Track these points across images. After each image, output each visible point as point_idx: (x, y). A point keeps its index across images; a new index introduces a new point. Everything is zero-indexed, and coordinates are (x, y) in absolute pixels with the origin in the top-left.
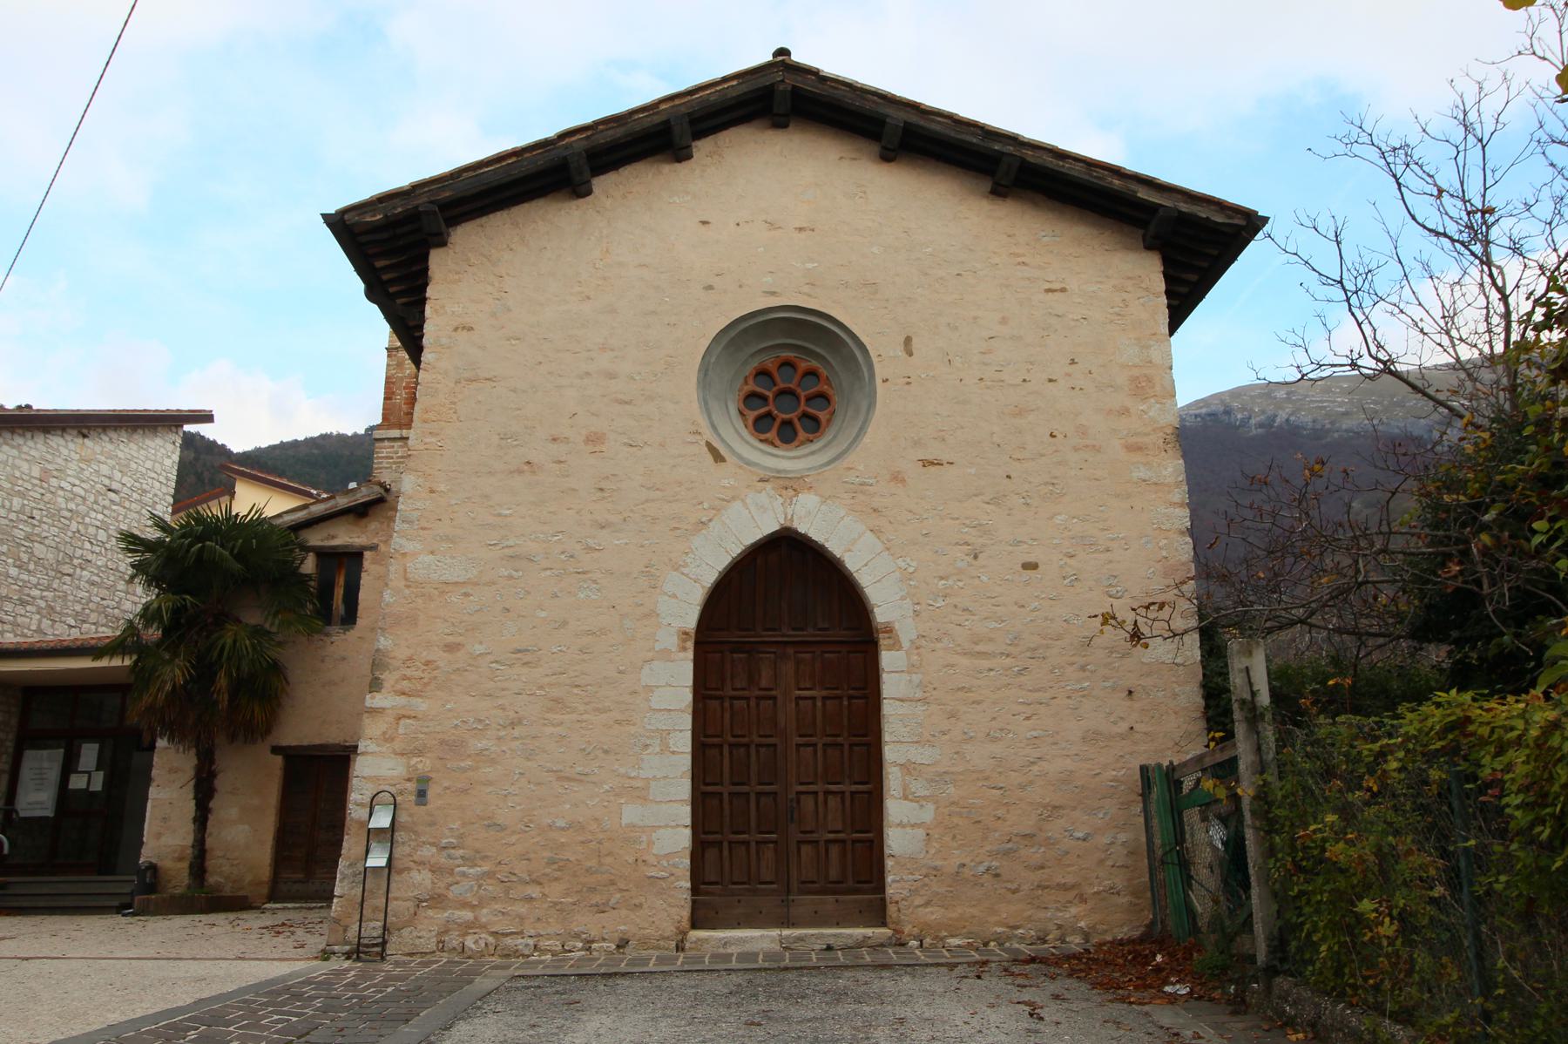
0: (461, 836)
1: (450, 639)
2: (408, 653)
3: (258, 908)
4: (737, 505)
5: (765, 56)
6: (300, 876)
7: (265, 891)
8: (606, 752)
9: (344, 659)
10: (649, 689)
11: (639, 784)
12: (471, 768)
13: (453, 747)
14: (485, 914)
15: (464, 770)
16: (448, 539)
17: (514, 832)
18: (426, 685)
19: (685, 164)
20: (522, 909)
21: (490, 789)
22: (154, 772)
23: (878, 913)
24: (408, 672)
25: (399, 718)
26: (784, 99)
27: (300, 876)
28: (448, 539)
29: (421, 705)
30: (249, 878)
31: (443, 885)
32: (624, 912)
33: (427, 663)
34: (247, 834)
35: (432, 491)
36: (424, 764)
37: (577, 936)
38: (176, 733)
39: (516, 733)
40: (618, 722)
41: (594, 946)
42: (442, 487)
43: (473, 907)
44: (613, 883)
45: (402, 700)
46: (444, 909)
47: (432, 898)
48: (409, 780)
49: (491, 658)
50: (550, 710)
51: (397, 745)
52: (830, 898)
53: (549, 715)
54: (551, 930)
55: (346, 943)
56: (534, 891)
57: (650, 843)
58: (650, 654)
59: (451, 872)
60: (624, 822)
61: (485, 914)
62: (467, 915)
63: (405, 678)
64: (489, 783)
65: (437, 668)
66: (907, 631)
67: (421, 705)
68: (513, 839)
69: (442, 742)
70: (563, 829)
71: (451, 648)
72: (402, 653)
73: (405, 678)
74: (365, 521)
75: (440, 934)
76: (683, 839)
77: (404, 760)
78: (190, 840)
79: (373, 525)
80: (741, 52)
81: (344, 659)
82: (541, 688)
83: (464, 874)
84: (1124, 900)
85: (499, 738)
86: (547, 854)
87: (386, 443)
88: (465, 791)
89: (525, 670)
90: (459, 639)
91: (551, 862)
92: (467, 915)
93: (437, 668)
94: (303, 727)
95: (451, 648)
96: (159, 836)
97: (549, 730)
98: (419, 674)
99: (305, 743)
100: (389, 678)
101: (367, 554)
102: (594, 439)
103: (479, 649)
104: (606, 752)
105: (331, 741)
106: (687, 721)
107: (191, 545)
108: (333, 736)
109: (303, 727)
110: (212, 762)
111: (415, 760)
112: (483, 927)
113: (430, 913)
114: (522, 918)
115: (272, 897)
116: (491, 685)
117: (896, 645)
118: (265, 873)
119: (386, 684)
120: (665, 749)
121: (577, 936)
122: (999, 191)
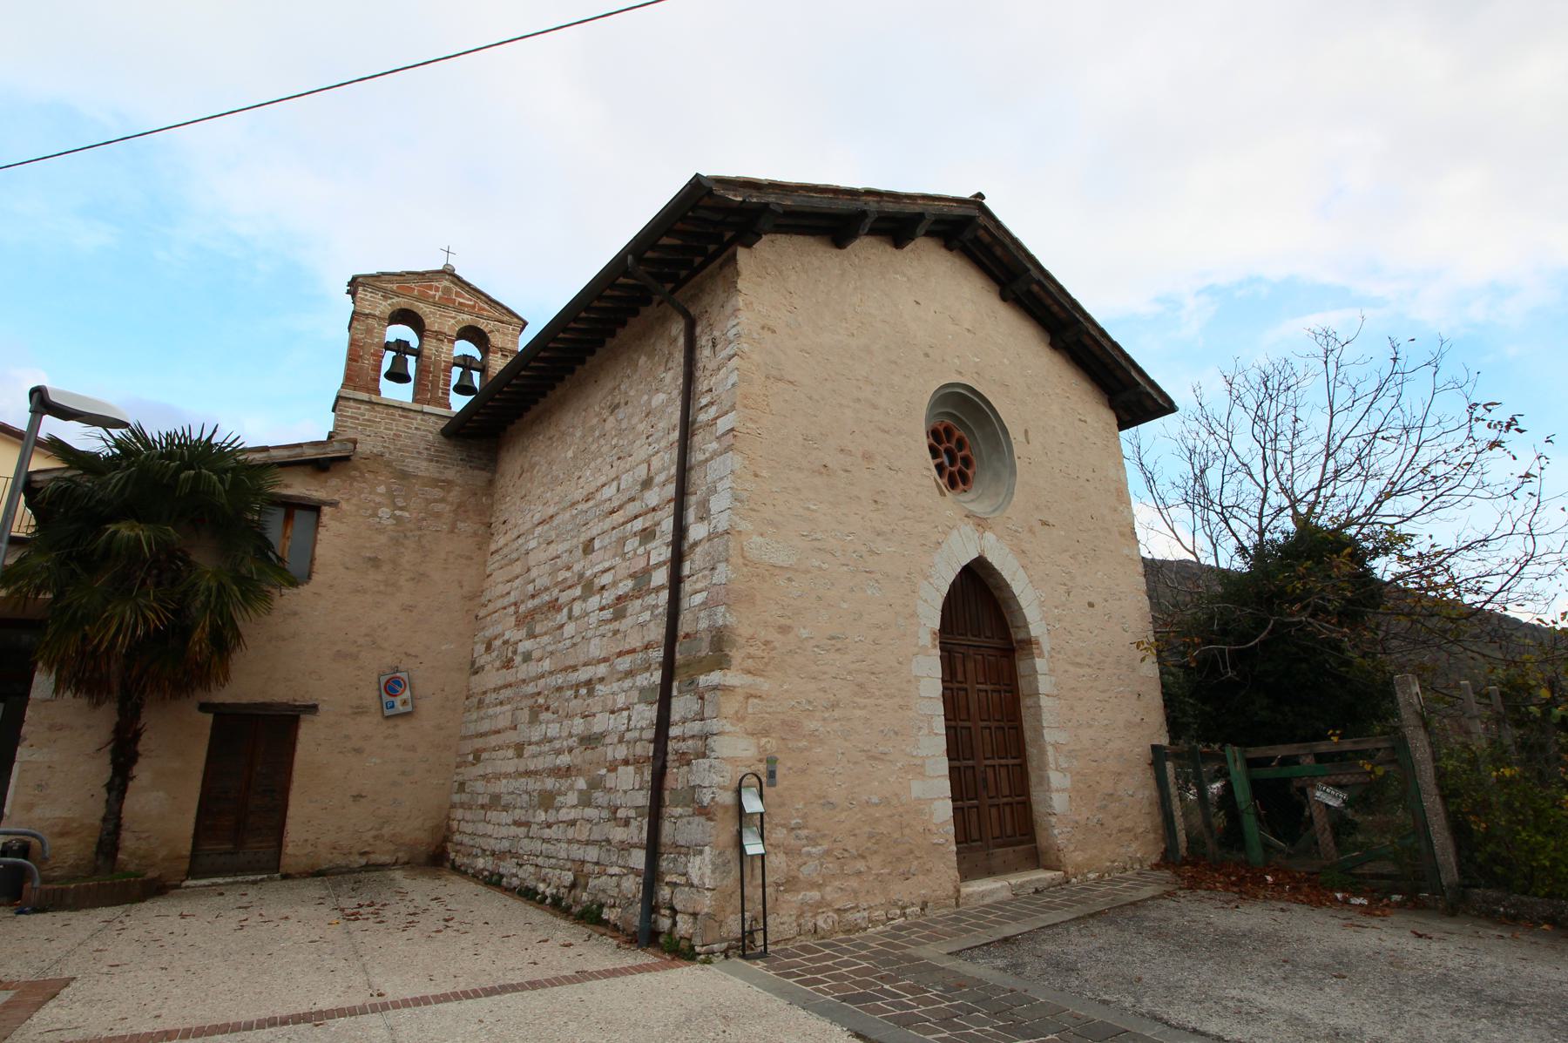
0: (804, 817)
1: (782, 621)
2: (750, 631)
3: (178, 887)
4: (955, 532)
5: (967, 194)
6: (228, 846)
7: (185, 866)
8: (896, 733)
9: (295, 613)
10: (918, 678)
11: (919, 762)
12: (806, 749)
13: (791, 727)
14: (830, 893)
15: (802, 750)
16: (771, 523)
17: (843, 810)
18: (767, 664)
19: (836, 251)
20: (854, 883)
21: (822, 769)
22: (25, 729)
23: (1036, 858)
24: (752, 651)
25: (749, 696)
26: (969, 235)
27: (228, 846)
28: (771, 523)
29: (764, 685)
30: (162, 853)
31: (794, 867)
32: (921, 877)
33: (766, 643)
34: (165, 803)
35: (756, 475)
36: (771, 744)
37: (895, 904)
38: (84, 679)
39: (836, 714)
40: (901, 707)
41: (908, 911)
42: (764, 473)
43: (819, 886)
44: (911, 852)
45: (748, 679)
46: (798, 892)
47: (788, 881)
48: (760, 761)
49: (813, 642)
50: (856, 694)
51: (749, 725)
52: (1010, 849)
53: (857, 699)
54: (877, 901)
55: (723, 940)
56: (860, 865)
57: (931, 814)
58: (916, 650)
59: (800, 854)
60: (914, 795)
61: (830, 893)
62: (815, 895)
63: (750, 656)
64: (820, 763)
65: (774, 649)
66: (1046, 643)
67: (764, 685)
68: (843, 816)
69: (783, 722)
70: (876, 805)
71: (784, 630)
72: (744, 631)
73: (750, 656)
74: (324, 476)
75: (798, 917)
76: (944, 810)
77: (753, 740)
78: (101, 811)
79: (334, 482)
80: (945, 180)
81: (295, 613)
82: (850, 673)
83: (809, 854)
84: (1151, 836)
85: (824, 719)
86: (867, 829)
87: (352, 403)
88: (803, 771)
89: (838, 656)
90: (788, 622)
91: (871, 836)
92: (815, 895)
93: (774, 649)
94: (247, 683)
95: (784, 630)
96: (30, 807)
97: (858, 713)
98: (759, 653)
99: (244, 701)
100: (736, 655)
101: (326, 509)
102: (867, 457)
103: (804, 633)
104: (896, 733)
105: (277, 699)
106: (940, 709)
107: (178, 470)
108: (280, 693)
109: (247, 683)
110: (137, 716)
111: (764, 740)
112: (829, 905)
113: (787, 896)
114: (855, 892)
115: (192, 873)
116: (815, 668)
117: (1041, 655)
118: (186, 848)
119: (734, 662)
120: (932, 733)
121: (895, 904)
122: (1054, 345)
